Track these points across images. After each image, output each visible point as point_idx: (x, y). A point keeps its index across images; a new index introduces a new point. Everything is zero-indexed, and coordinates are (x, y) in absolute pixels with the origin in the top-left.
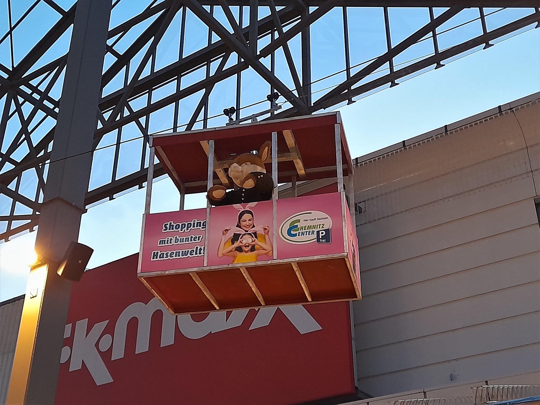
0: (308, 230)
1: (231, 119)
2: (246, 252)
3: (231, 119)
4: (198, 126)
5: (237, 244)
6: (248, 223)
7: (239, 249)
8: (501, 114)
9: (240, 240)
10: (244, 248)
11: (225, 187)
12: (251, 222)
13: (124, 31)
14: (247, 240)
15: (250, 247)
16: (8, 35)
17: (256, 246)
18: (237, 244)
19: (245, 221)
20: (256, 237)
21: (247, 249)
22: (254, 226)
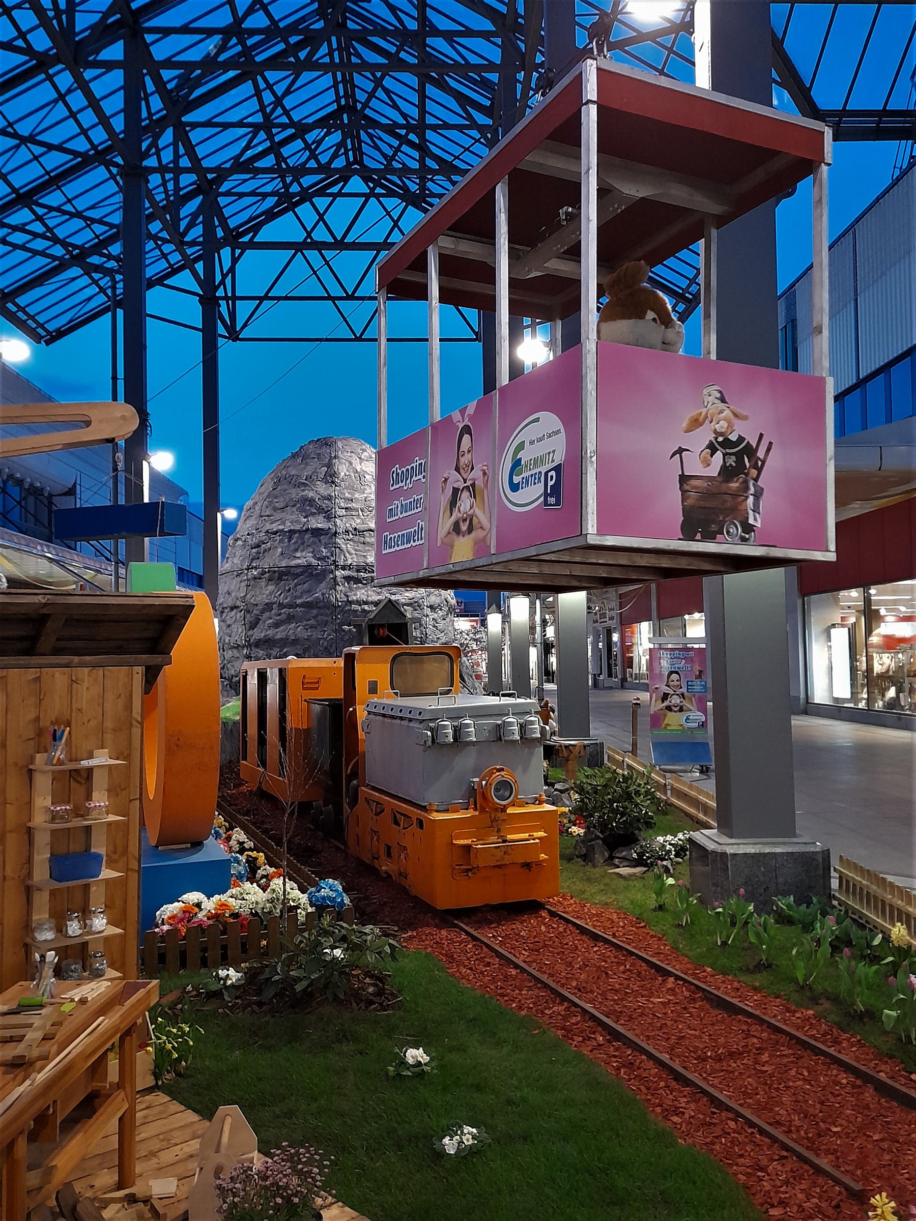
0: (537, 471)
1: (157, 1083)
2: (675, 712)
3: (157, 1083)
4: (149, 38)
5: (666, 703)
6: (676, 683)
7: (669, 708)
8: (364, 556)
9: (669, 699)
10: (673, 708)
11: (747, 1167)
12: (679, 683)
13: (503, 390)
14: (676, 700)
15: (678, 708)
16: (39, 141)
17: (684, 708)
18: (666, 703)
19: (673, 681)
20: (684, 698)
21: (676, 709)
22: (681, 688)
